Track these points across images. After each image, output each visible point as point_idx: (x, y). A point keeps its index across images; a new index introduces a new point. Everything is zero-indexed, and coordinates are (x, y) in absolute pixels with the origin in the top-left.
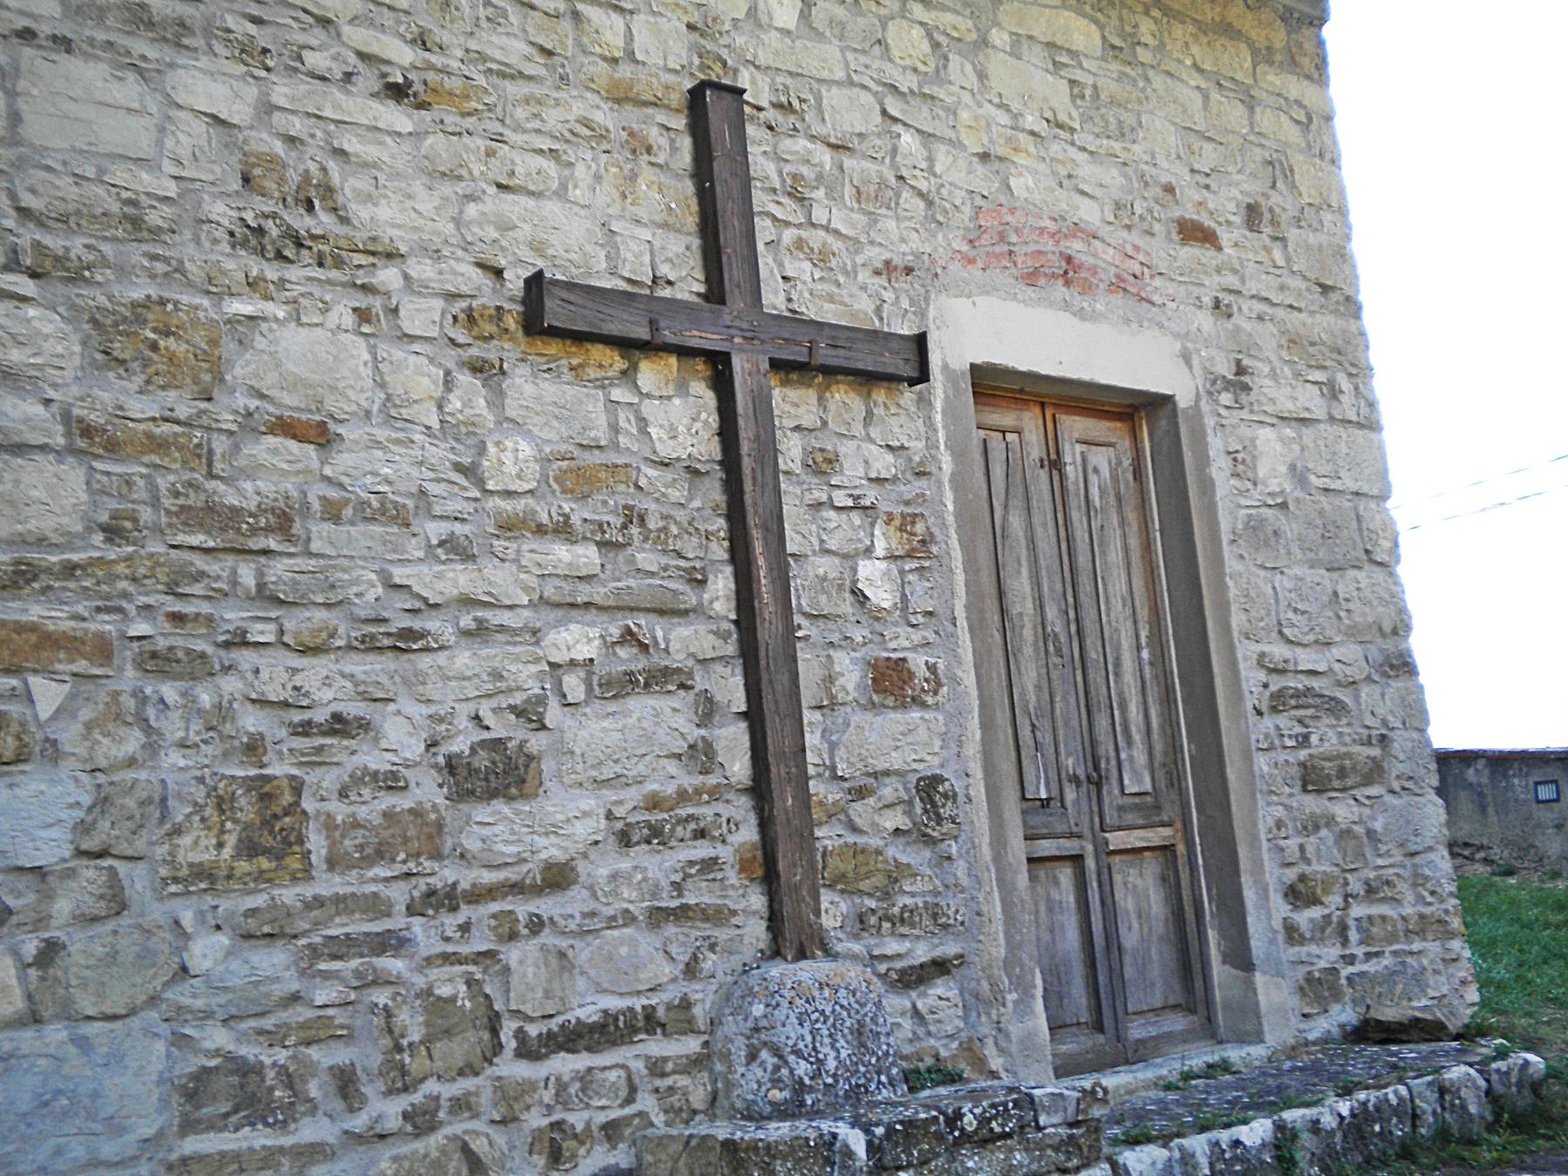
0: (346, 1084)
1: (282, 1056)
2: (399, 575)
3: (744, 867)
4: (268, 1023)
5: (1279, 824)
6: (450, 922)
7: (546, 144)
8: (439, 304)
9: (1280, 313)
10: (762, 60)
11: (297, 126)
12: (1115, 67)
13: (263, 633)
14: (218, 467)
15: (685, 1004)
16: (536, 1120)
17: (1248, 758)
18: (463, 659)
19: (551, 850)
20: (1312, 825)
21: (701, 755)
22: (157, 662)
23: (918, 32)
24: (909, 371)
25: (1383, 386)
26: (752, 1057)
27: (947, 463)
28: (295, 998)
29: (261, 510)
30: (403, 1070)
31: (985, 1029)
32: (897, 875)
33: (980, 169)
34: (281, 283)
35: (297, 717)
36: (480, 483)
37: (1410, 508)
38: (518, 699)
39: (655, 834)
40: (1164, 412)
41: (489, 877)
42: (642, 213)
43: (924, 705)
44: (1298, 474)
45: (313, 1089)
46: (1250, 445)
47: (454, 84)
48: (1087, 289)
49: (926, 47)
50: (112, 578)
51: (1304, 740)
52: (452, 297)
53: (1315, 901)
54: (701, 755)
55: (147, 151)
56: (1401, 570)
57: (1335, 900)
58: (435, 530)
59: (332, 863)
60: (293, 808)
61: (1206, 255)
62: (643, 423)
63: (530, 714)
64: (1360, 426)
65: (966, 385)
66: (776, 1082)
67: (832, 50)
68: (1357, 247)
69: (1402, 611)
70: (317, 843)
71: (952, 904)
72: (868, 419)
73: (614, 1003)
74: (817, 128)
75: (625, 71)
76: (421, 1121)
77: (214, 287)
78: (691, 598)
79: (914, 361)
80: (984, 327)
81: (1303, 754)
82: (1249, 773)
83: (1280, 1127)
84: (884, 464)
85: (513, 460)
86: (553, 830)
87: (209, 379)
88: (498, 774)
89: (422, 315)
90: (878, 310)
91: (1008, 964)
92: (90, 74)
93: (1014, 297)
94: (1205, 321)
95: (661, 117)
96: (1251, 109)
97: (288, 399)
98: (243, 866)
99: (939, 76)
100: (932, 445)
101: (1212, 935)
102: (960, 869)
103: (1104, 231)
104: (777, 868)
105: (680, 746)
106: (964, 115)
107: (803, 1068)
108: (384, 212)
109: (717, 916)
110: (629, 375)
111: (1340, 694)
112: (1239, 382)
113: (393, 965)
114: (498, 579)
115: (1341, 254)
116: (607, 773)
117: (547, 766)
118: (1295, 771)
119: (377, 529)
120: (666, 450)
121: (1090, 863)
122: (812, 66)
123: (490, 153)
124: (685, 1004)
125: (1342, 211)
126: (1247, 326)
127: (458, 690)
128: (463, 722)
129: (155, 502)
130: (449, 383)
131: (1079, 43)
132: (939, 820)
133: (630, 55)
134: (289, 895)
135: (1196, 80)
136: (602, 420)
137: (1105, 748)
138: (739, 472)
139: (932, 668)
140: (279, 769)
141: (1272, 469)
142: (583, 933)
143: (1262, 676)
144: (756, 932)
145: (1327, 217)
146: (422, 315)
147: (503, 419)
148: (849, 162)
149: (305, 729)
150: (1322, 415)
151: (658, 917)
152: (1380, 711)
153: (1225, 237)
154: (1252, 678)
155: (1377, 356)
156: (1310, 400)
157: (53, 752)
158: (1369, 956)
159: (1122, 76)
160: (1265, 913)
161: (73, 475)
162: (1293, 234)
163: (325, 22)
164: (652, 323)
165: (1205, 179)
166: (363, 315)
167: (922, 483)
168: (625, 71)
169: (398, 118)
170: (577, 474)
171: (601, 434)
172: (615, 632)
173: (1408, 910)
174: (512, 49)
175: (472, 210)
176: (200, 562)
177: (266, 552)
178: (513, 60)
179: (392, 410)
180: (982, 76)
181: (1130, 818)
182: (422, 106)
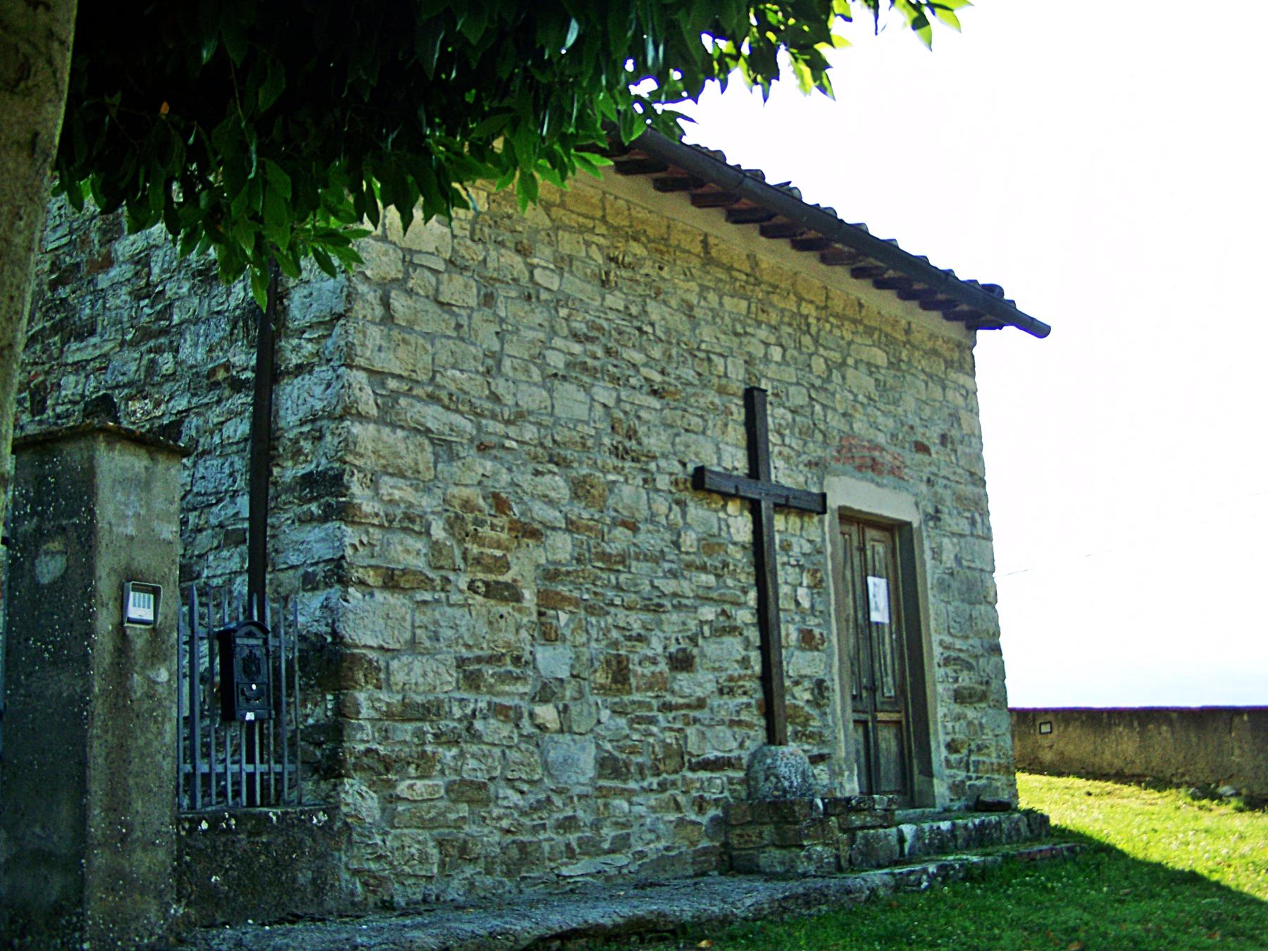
0: (641, 768)
1: (624, 756)
2: (656, 583)
3: (759, 707)
4: (620, 744)
5: (945, 716)
6: (671, 716)
7: (699, 413)
8: (667, 477)
9: (953, 485)
10: (770, 375)
11: (628, 407)
12: (892, 372)
13: (618, 601)
14: (606, 538)
15: (739, 758)
16: (695, 794)
17: (934, 685)
18: (674, 617)
19: (700, 693)
20: (958, 718)
21: (745, 662)
22: (590, 610)
23: (822, 360)
24: (820, 509)
25: (994, 520)
26: (767, 779)
27: (829, 549)
28: (627, 736)
29: (618, 555)
30: (658, 769)
31: (836, 785)
32: (808, 718)
33: (843, 420)
34: (623, 468)
35: (628, 633)
36: (679, 548)
37: (1004, 581)
38: (689, 633)
39: (731, 692)
40: (907, 528)
41: (681, 701)
42: (729, 440)
43: (818, 650)
44: (958, 559)
45: (632, 769)
46: (940, 546)
47: (672, 389)
48: (880, 473)
49: (824, 366)
50: (578, 577)
51: (956, 680)
52: (671, 474)
53: (957, 751)
54: (745, 662)
55: (586, 418)
56: (997, 606)
57: (965, 751)
58: (667, 566)
59: (638, 689)
60: (627, 667)
61: (925, 458)
62: (728, 526)
63: (693, 640)
64: (984, 538)
65: (837, 515)
66: (776, 789)
67: (792, 370)
68: (985, 454)
69: (997, 625)
70: (633, 681)
71: (826, 733)
72: (802, 528)
73: (720, 754)
74: (787, 404)
75: (724, 381)
76: (663, 787)
77: (605, 471)
78: (742, 599)
79: (820, 505)
80: (848, 491)
81: (956, 686)
82: (935, 691)
83: (954, 825)
84: (807, 548)
86: (700, 685)
88: (682, 662)
89: (663, 482)
90: (806, 482)
91: (846, 759)
92: (570, 388)
93: (853, 477)
94: (923, 488)
95: (735, 400)
96: (944, 389)
97: (626, 513)
98: (614, 686)
99: (828, 379)
100: (824, 540)
101: (915, 761)
102: (830, 718)
103: (887, 447)
104: (770, 708)
105: (739, 658)
106: (838, 396)
107: (786, 784)
108: (652, 441)
109: (750, 725)
110: (724, 507)
111: (971, 660)
112: (936, 517)
113: (655, 729)
114: (686, 587)
115: (979, 458)
116: (717, 665)
117: (697, 660)
118: (952, 693)
119: (649, 564)
120: (737, 538)
121: (870, 724)
122: (786, 377)
123: (683, 417)
124: (739, 758)
125: (980, 437)
126: (940, 490)
128: (673, 641)
129: (589, 551)
130: (670, 509)
131: (879, 363)
132: (823, 697)
133: (726, 375)
134: (626, 698)
135: (923, 377)
136: (716, 526)
137: (878, 675)
138: (760, 549)
139: (821, 634)
140: (622, 652)
141: (948, 558)
142: (710, 726)
143: (941, 650)
144: (761, 735)
145: (974, 440)
146: (663, 482)
147: (685, 523)
148: (798, 418)
149: (629, 638)
150: (968, 532)
151: (732, 723)
152: (987, 670)
153: (933, 451)
154: (937, 650)
155: (992, 506)
156: (965, 526)
157: (564, 640)
158: (978, 778)
159: (895, 376)
160: (939, 754)
161: (567, 537)
162: (960, 448)
163: (634, 365)
164: (737, 488)
165: (926, 423)
166: (645, 481)
167: (819, 557)
168: (724, 381)
169: (655, 403)
171: (715, 531)
172: (719, 610)
173: (994, 760)
174: (690, 374)
175: (678, 440)
176: (599, 573)
177: (618, 571)
178: (690, 378)
179: (652, 518)
180: (844, 378)
181: (886, 707)
182: (662, 398)
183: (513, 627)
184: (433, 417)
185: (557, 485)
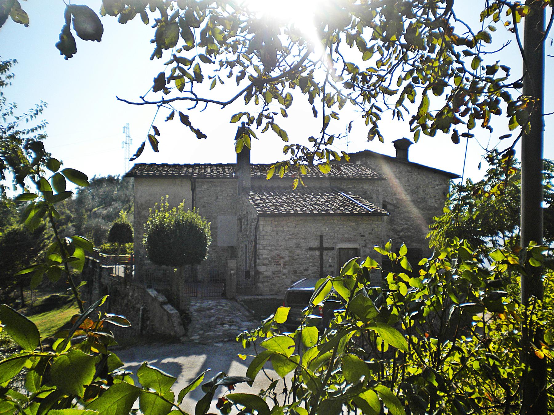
85: (308, 256)
87: (294, 253)
88: (306, 270)
112: (365, 246)
127: (305, 266)
170: (312, 256)
183: (279, 268)
184: (269, 248)
185: (287, 252)
